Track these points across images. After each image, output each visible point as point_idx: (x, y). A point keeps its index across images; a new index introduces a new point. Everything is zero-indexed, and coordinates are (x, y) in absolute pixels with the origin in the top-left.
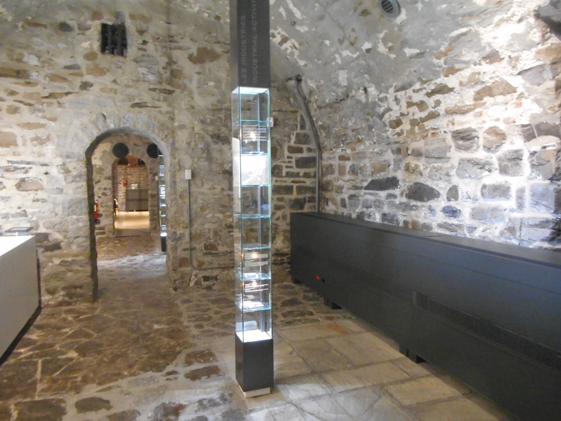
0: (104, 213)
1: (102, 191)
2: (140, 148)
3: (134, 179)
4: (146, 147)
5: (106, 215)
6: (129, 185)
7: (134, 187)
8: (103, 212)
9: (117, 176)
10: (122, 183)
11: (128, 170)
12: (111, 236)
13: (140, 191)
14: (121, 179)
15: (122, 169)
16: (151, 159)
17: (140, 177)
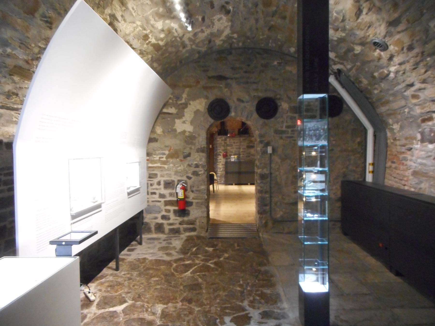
0: (194, 201)
1: (193, 169)
2: (245, 104)
3: (233, 151)
4: (255, 103)
5: (197, 203)
6: (228, 157)
7: (233, 158)
8: (193, 199)
9: (217, 147)
10: (222, 154)
11: (228, 141)
12: (203, 234)
13: (239, 163)
14: (220, 150)
15: (222, 140)
16: (261, 121)
17: (240, 148)
